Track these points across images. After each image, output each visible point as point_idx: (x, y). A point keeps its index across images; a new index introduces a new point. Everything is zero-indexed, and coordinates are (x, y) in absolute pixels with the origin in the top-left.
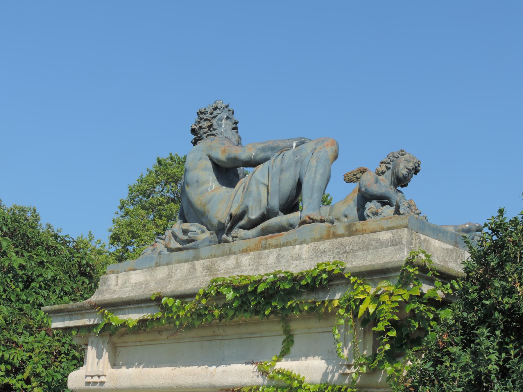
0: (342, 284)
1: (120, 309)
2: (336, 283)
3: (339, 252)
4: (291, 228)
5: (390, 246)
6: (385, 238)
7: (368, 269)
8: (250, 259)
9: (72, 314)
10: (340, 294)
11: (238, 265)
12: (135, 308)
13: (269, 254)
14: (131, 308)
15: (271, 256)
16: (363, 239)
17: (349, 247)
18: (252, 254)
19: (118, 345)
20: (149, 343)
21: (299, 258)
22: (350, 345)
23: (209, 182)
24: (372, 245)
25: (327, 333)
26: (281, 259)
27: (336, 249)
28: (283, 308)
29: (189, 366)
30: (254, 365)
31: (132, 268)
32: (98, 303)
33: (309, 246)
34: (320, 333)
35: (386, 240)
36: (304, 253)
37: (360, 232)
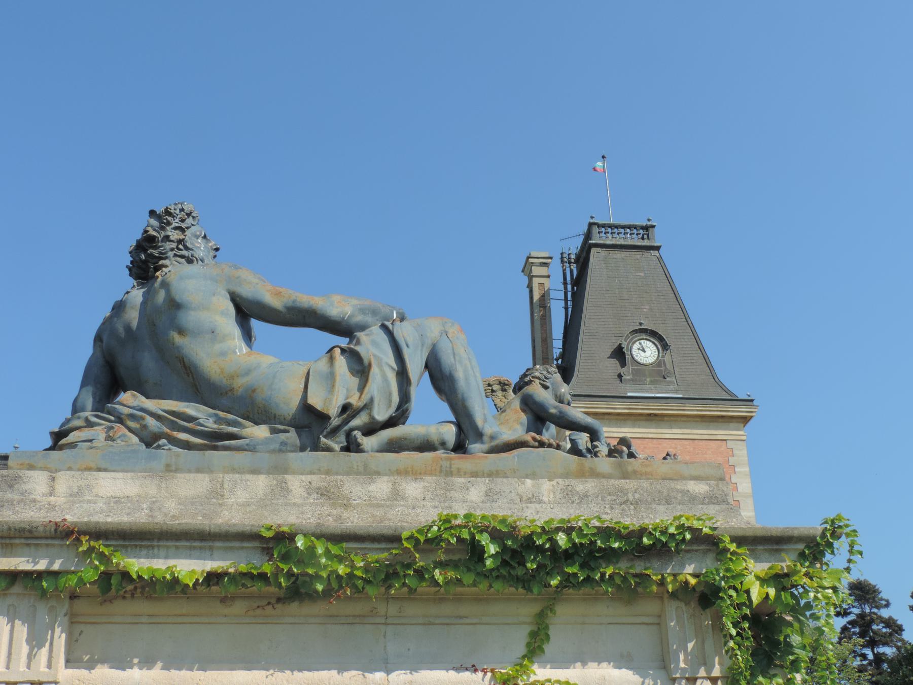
0: (696, 551)
1: (141, 546)
4: (440, 447)
5: (708, 503)
6: (697, 491)
7: (760, 533)
8: (424, 487)
9: (12, 545)
10: (60, 561)
11: (396, 495)
12: (191, 548)
13: (469, 485)
14: (177, 547)
15: (472, 489)
17: (633, 495)
20: (180, 620)
22: (690, 646)
23: (234, 339)
28: (588, 579)
29: (300, 670)
30: (480, 674)
31: (93, 465)
32: (84, 528)
33: (554, 483)
36: (545, 493)
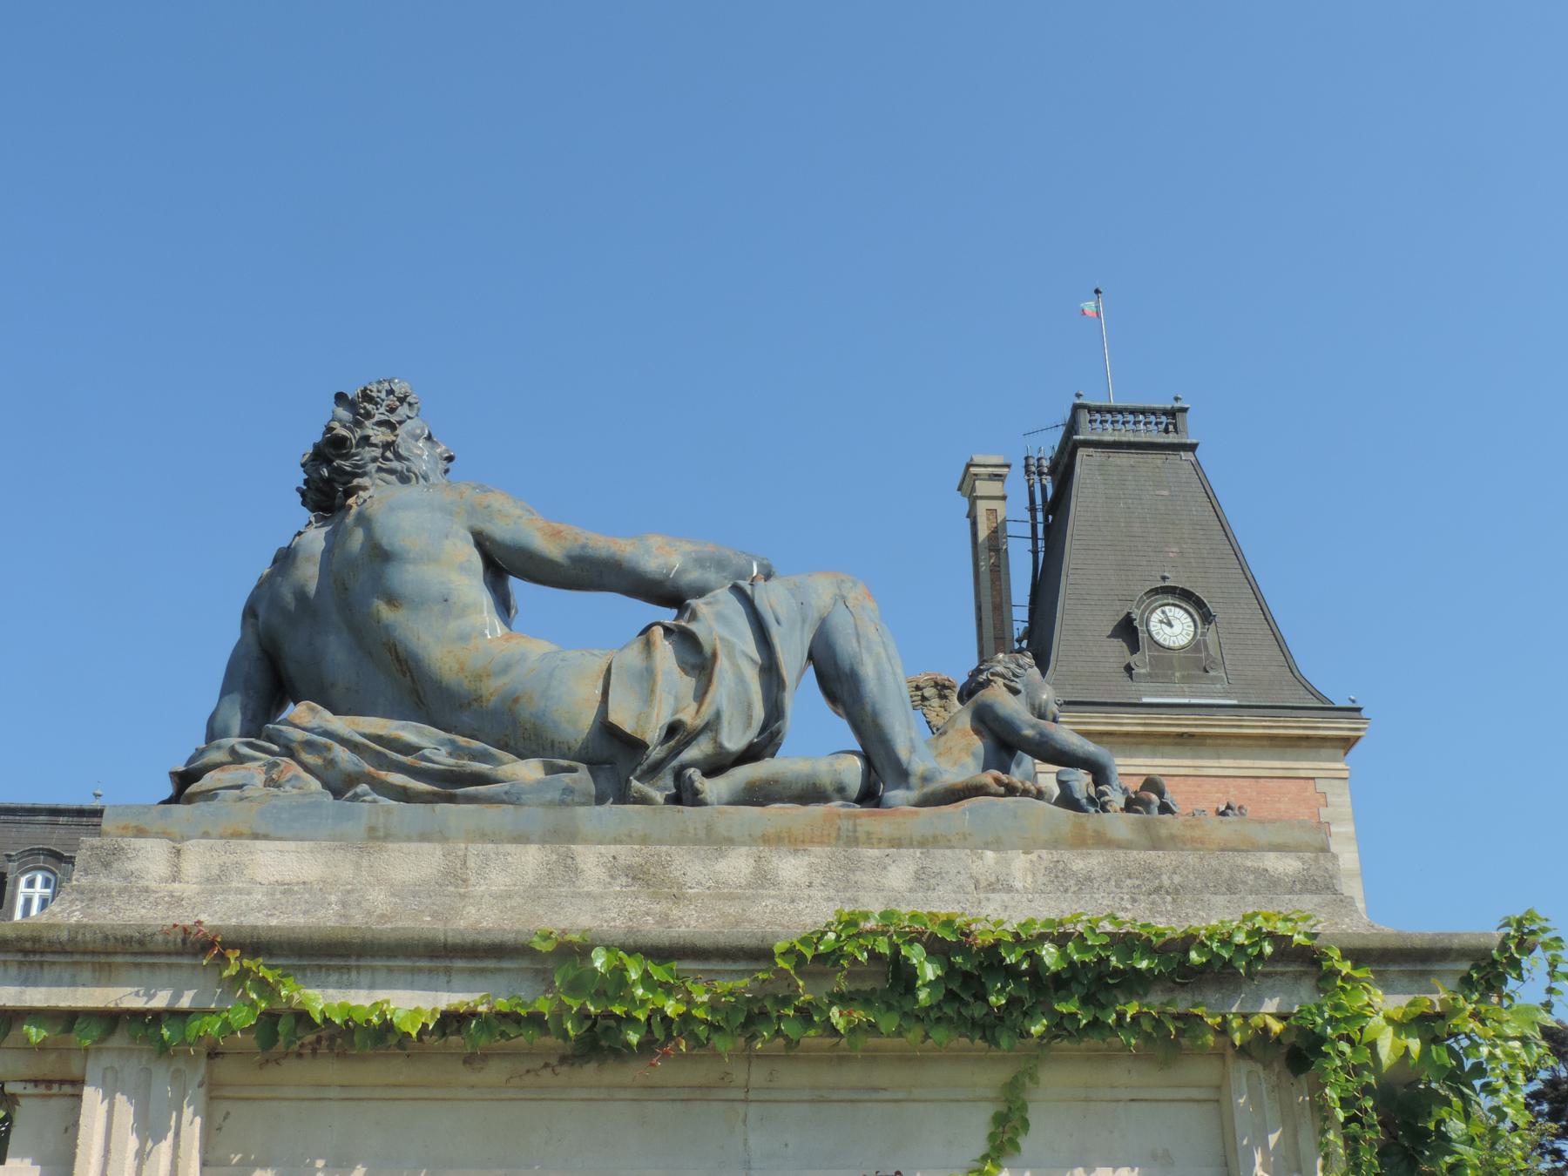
6: (1281, 870)
8: (810, 865)
9: (110, 965)
11: (763, 879)
13: (887, 860)
15: (892, 868)
19: (226, 1092)
20: (394, 1093)
21: (998, 885)
22: (1273, 1139)
24: (1245, 883)
25: (1143, 1104)
28: (1095, 1024)
33: (1033, 857)
34: (1118, 1101)
36: (1019, 875)
37: (1184, 843)
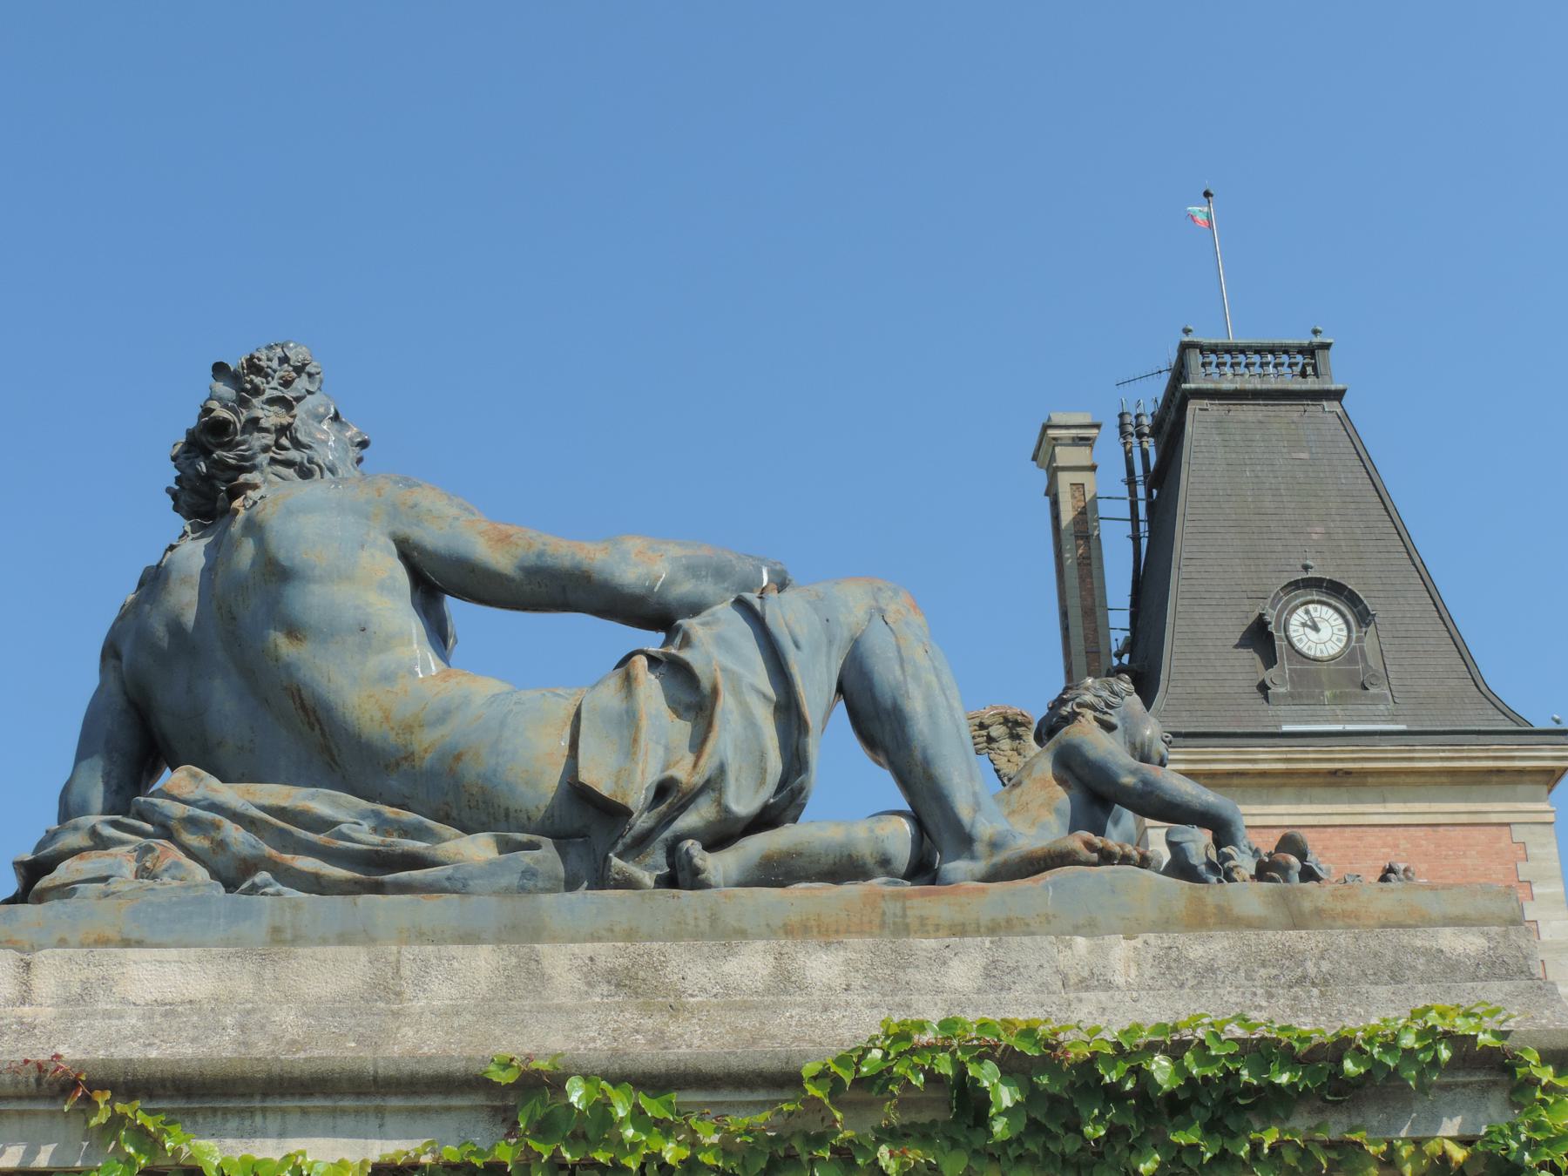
0: (1465, 1085)
2: (278, 1104)
3: (1276, 977)
5: (1487, 978)
6: (1460, 950)
8: (847, 962)
10: (50, 1148)
11: (785, 981)
13: (947, 953)
15: (955, 963)
16: (1373, 943)
17: (1317, 965)
18: (858, 946)
24: (1413, 968)
26: (1006, 978)
27: (1264, 965)
28: (1223, 1157)
33: (1138, 943)
35: (1468, 956)
36: (1119, 967)
